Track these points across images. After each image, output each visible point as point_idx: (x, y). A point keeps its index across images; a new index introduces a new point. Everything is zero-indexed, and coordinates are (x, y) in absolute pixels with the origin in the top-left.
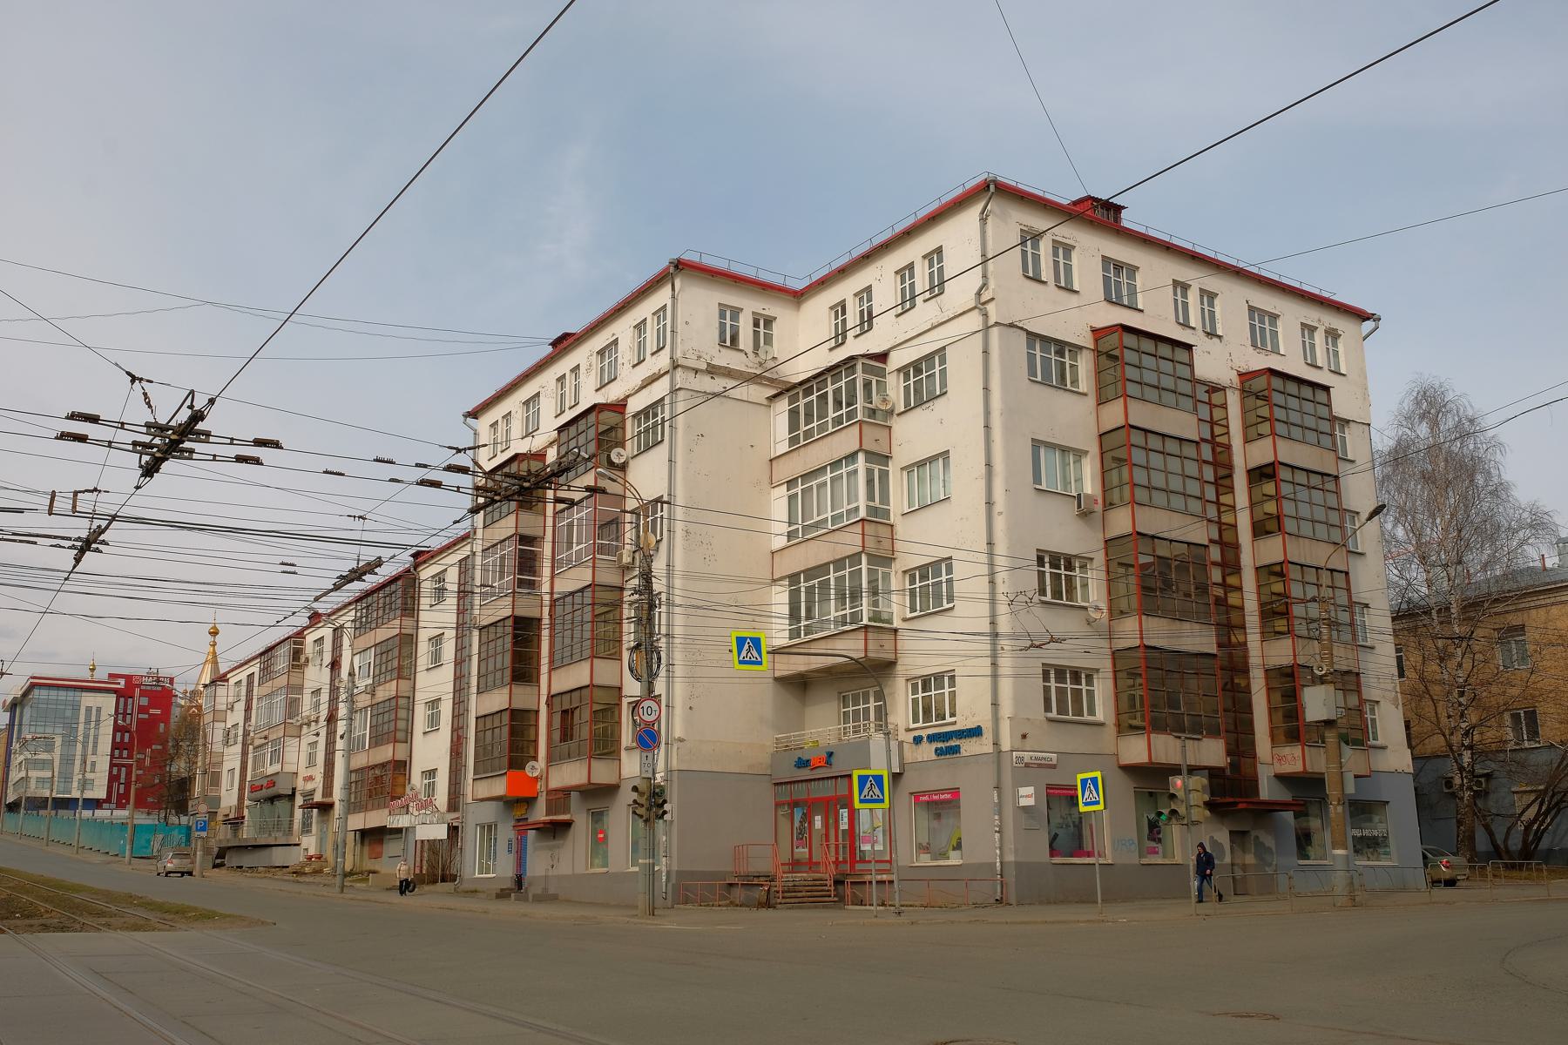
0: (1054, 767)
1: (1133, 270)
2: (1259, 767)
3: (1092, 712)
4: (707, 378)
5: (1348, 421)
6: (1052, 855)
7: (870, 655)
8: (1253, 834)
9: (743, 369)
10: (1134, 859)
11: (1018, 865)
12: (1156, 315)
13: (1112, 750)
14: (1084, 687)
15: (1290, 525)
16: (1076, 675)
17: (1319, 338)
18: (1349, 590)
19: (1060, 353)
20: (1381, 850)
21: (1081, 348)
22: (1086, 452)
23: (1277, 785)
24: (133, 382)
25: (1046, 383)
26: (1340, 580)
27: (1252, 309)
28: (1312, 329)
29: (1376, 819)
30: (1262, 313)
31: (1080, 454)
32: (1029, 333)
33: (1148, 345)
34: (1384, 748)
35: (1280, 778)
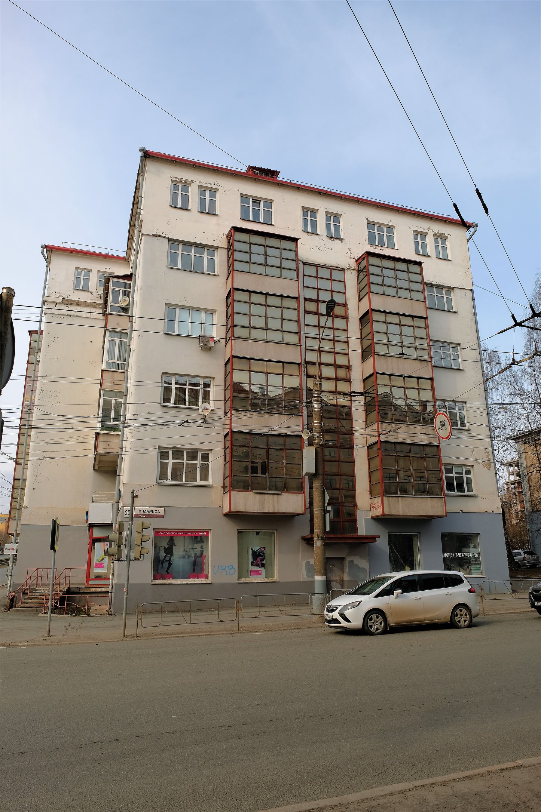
0: (163, 516)
1: (269, 203)
2: (358, 513)
3: (205, 477)
4: (64, 307)
5: (453, 288)
6: (155, 578)
7: (232, 510)
8: (348, 559)
9: (90, 301)
10: (233, 578)
11: (116, 584)
12: (404, 249)
13: (218, 504)
14: (199, 462)
15: (378, 349)
16: (192, 455)
17: (430, 240)
18: (433, 390)
19: (448, 293)
20: (473, 567)
21: (217, 248)
22: (215, 311)
23: (374, 524)
24: (136, 496)
25: (185, 269)
26: (426, 384)
27: (371, 224)
28: (424, 235)
29: (472, 545)
30: (381, 226)
31: (210, 312)
32: (170, 240)
33: (403, 266)
34: (476, 496)
35: (376, 519)
